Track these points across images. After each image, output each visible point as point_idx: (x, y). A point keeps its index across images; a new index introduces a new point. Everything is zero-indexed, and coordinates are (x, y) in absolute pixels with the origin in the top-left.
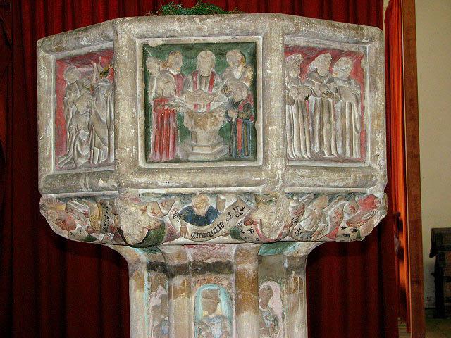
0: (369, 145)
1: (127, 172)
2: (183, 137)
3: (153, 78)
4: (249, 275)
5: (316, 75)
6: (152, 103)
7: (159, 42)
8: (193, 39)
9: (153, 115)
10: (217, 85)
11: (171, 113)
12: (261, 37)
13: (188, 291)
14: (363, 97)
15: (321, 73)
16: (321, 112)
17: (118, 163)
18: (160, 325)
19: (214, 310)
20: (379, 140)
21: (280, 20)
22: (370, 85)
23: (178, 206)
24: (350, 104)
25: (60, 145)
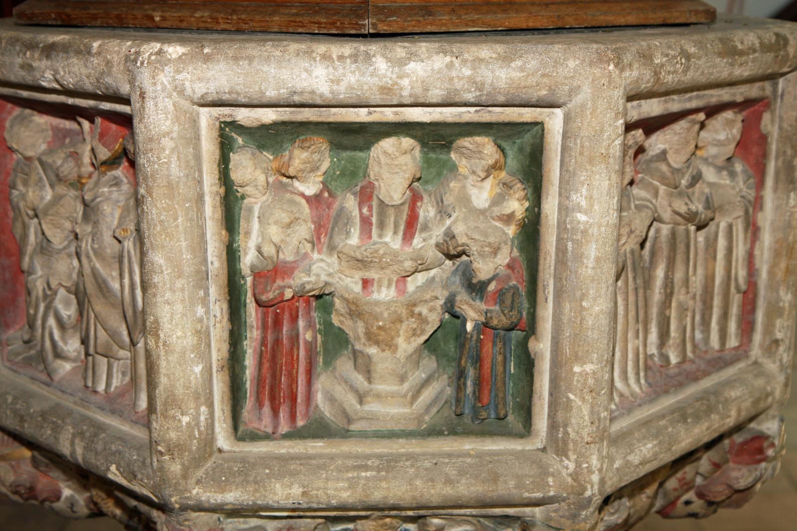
0: (760, 316)
1: (185, 477)
2: (330, 356)
3: (250, 210)
5: (664, 168)
7: (269, 116)
9: (252, 312)
10: (425, 228)
11: (301, 305)
14: (758, 203)
17: (161, 453)
20: (787, 305)
21: (622, 70)
24: (730, 227)
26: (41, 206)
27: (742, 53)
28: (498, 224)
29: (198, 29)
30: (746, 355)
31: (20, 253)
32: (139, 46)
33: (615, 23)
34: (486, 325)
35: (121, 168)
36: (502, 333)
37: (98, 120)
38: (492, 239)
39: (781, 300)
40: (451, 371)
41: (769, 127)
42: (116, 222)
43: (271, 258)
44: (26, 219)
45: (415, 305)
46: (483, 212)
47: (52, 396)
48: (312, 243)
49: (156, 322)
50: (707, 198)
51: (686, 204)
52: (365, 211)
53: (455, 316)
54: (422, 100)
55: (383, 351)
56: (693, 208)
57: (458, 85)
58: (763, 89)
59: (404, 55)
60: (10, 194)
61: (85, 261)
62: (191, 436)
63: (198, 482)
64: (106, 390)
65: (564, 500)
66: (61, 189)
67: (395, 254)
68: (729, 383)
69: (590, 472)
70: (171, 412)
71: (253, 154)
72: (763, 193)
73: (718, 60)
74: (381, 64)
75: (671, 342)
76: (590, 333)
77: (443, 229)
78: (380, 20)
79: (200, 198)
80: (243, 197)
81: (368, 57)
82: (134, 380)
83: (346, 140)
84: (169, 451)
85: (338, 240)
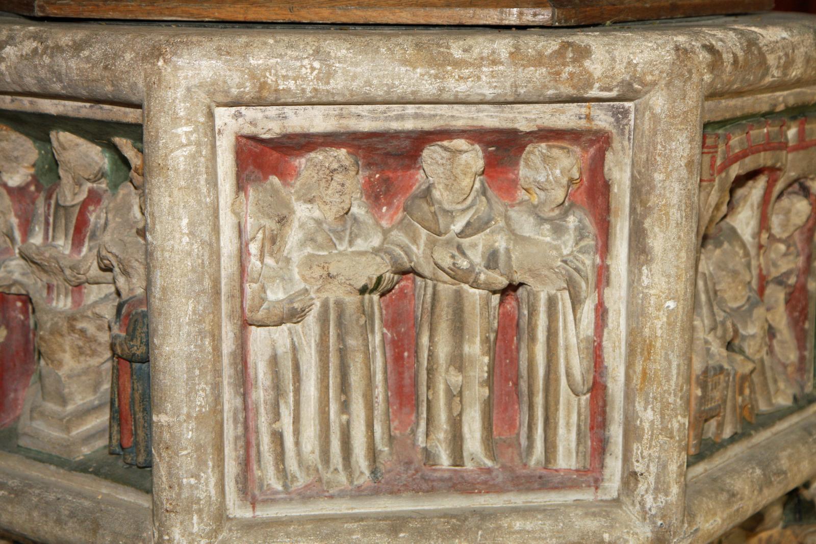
24: (552, 303)
33: (379, 21)
39: (638, 417)
51: (453, 257)
58: (588, 117)
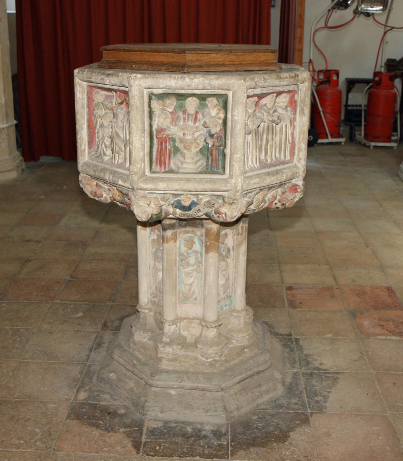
0: (296, 151)
1: (138, 180)
2: (175, 154)
3: (156, 115)
4: (214, 231)
5: (265, 108)
6: (155, 133)
7: (161, 91)
8: (184, 90)
9: (155, 141)
11: (168, 139)
12: (231, 92)
13: (175, 238)
14: (295, 119)
15: (269, 106)
16: (268, 134)
17: (132, 175)
18: (156, 252)
19: (191, 249)
20: (303, 148)
21: (245, 82)
22: (300, 111)
23: (172, 200)
24: (286, 125)
25: (91, 142)
26: (102, 115)
27: (283, 79)
28: (217, 120)
29: (144, 70)
30: (292, 162)
31: (95, 128)
32: (131, 74)
34: (213, 145)
35: (123, 105)
36: (218, 147)
37: (118, 92)
38: (215, 123)
40: (206, 158)
41: (297, 98)
42: (122, 119)
43: (160, 127)
44: (97, 119)
45: (196, 140)
46: (214, 117)
47: (103, 165)
48: (171, 124)
49: (132, 141)
50: (278, 117)
52: (184, 116)
53: (207, 143)
54: (197, 88)
55: (188, 151)
56: (274, 119)
57: (206, 85)
58: (294, 88)
59: (193, 77)
60: (93, 112)
61: (114, 129)
62: (140, 170)
63: (141, 182)
64: (118, 163)
65: (232, 190)
66: (107, 111)
67: (191, 127)
68: (285, 169)
69: (239, 183)
70: (135, 164)
71: (157, 101)
72: (296, 116)
73: (275, 80)
74: (187, 79)
75: (268, 156)
76: (238, 147)
77: (204, 121)
78: (188, 69)
79: (144, 111)
80: (154, 112)
81: (184, 78)
82: (125, 159)
83: (180, 98)
84: (134, 174)
85: (177, 123)
